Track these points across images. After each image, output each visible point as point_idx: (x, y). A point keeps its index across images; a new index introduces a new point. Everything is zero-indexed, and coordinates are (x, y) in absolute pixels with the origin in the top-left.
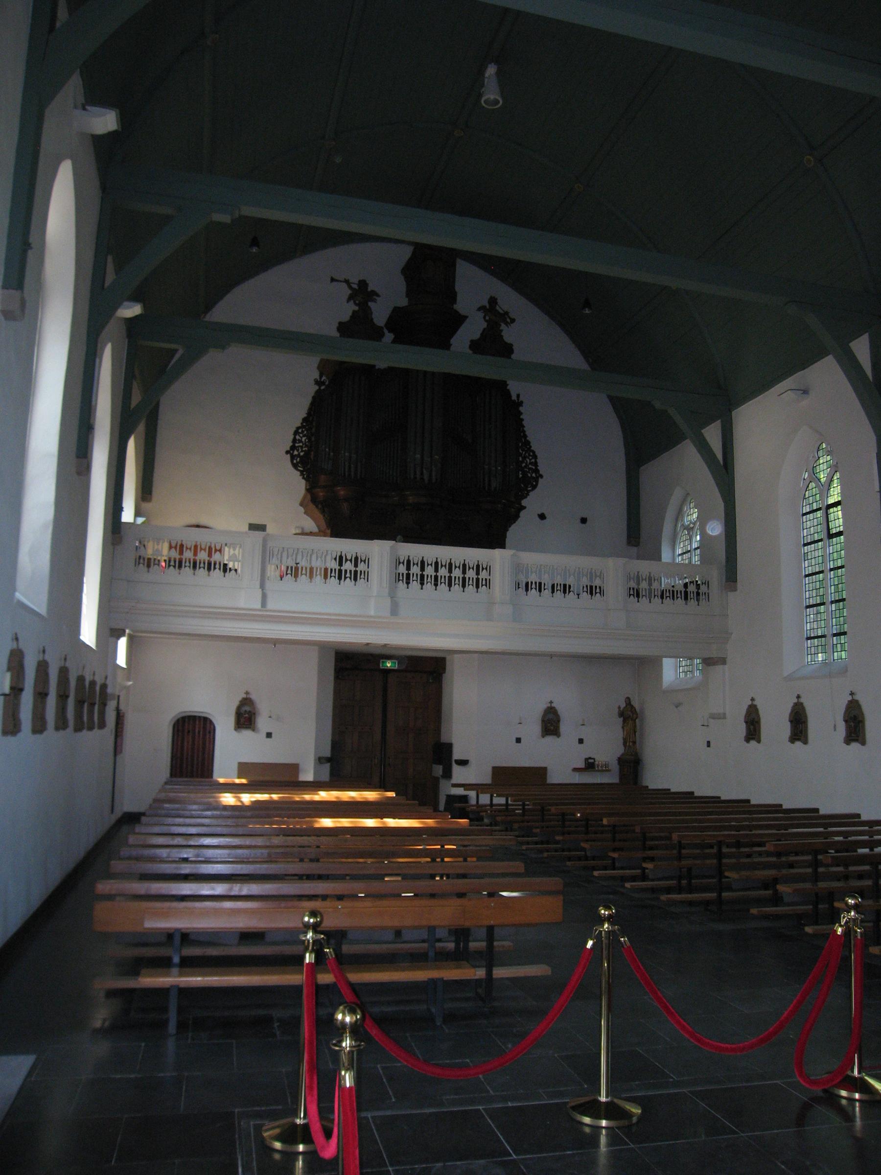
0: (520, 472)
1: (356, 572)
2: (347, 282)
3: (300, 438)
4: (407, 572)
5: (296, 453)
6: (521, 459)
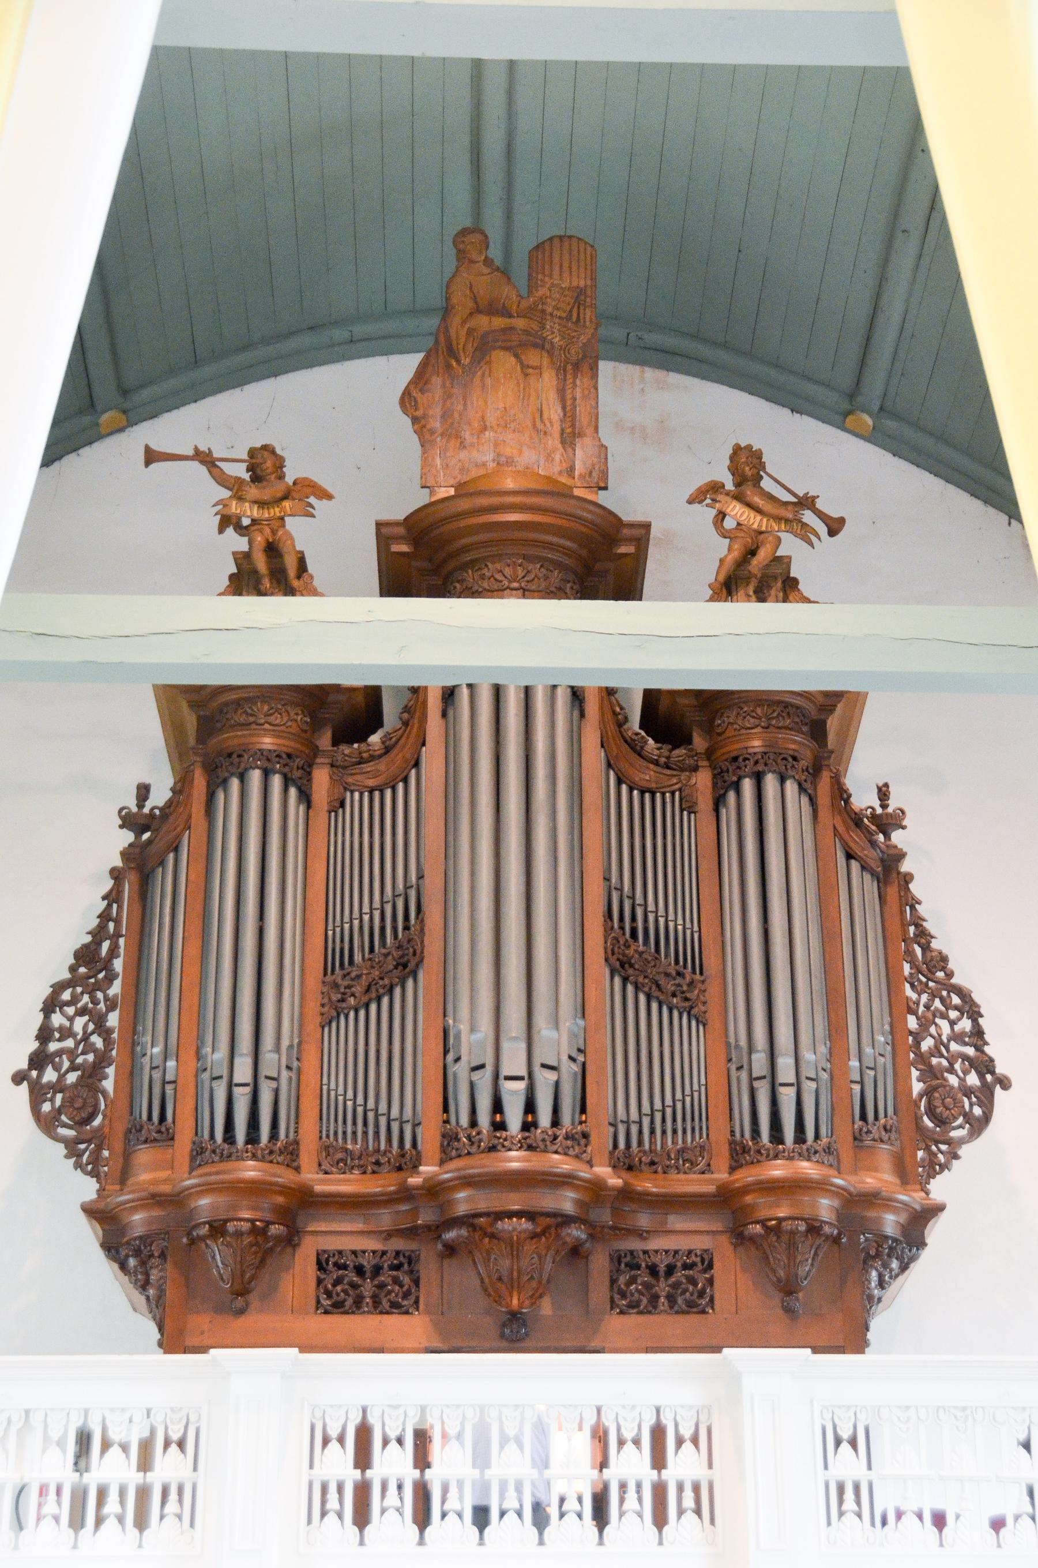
0: (915, 1073)
2: (206, 459)
3: (67, 1024)
5: (50, 1075)
6: (912, 1023)
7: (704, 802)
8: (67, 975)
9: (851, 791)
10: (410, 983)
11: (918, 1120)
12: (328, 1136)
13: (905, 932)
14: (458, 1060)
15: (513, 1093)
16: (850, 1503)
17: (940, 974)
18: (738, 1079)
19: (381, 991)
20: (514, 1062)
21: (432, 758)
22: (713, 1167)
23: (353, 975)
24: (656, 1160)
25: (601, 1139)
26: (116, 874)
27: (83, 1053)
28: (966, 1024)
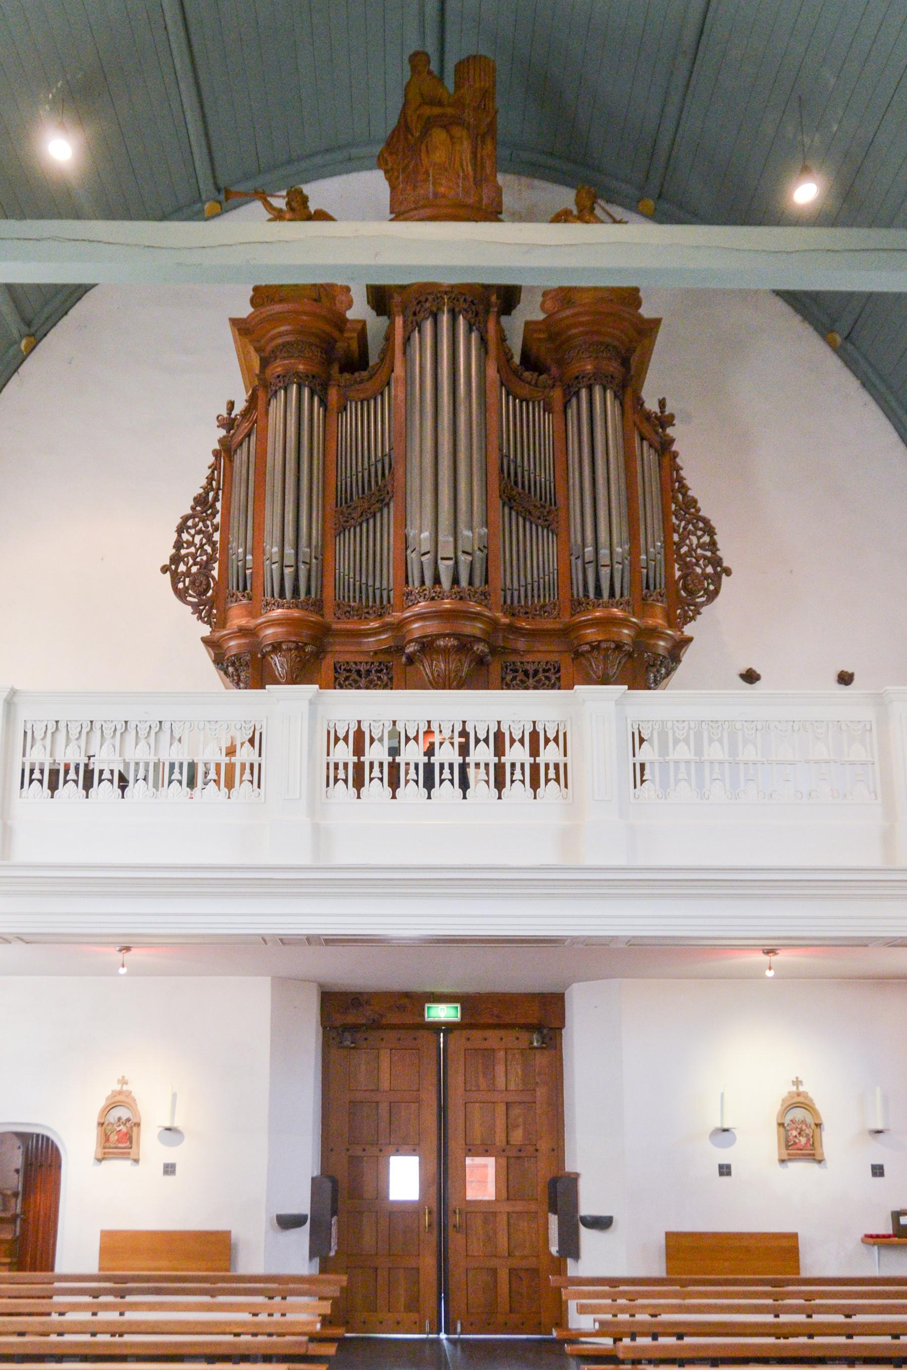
0: (677, 566)
3: (191, 539)
4: (355, 759)
5: (182, 568)
6: (676, 537)
7: (558, 406)
8: (190, 512)
9: (645, 398)
10: (385, 511)
11: (678, 591)
12: (339, 598)
13: (673, 486)
15: (445, 568)
17: (693, 510)
18: (576, 563)
19: (368, 515)
20: (446, 550)
21: (399, 370)
22: (561, 616)
23: (353, 506)
24: (528, 610)
25: (497, 598)
26: (216, 454)
27: (200, 555)
28: (706, 539)
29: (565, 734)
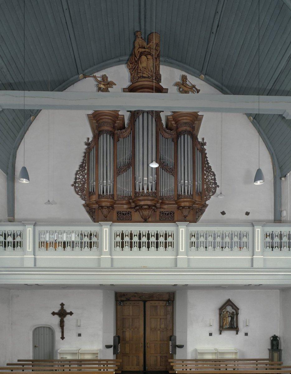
1: (91, 243)
4: (122, 241)
5: (77, 185)
14: (137, 181)
16: (193, 245)
17: (210, 169)
26: (85, 153)
28: (213, 177)
29: (173, 234)
